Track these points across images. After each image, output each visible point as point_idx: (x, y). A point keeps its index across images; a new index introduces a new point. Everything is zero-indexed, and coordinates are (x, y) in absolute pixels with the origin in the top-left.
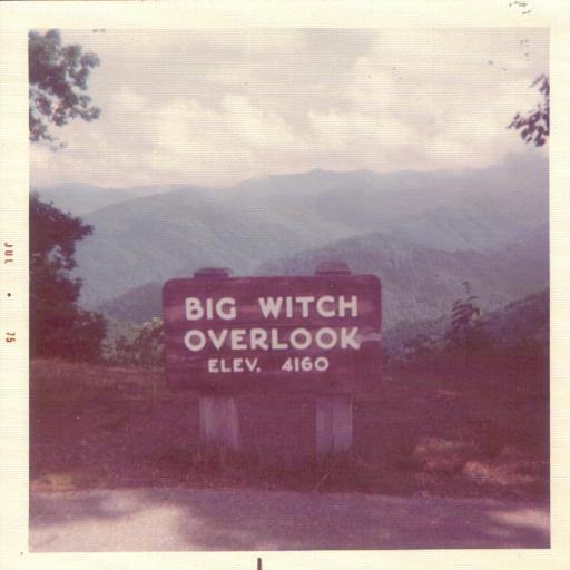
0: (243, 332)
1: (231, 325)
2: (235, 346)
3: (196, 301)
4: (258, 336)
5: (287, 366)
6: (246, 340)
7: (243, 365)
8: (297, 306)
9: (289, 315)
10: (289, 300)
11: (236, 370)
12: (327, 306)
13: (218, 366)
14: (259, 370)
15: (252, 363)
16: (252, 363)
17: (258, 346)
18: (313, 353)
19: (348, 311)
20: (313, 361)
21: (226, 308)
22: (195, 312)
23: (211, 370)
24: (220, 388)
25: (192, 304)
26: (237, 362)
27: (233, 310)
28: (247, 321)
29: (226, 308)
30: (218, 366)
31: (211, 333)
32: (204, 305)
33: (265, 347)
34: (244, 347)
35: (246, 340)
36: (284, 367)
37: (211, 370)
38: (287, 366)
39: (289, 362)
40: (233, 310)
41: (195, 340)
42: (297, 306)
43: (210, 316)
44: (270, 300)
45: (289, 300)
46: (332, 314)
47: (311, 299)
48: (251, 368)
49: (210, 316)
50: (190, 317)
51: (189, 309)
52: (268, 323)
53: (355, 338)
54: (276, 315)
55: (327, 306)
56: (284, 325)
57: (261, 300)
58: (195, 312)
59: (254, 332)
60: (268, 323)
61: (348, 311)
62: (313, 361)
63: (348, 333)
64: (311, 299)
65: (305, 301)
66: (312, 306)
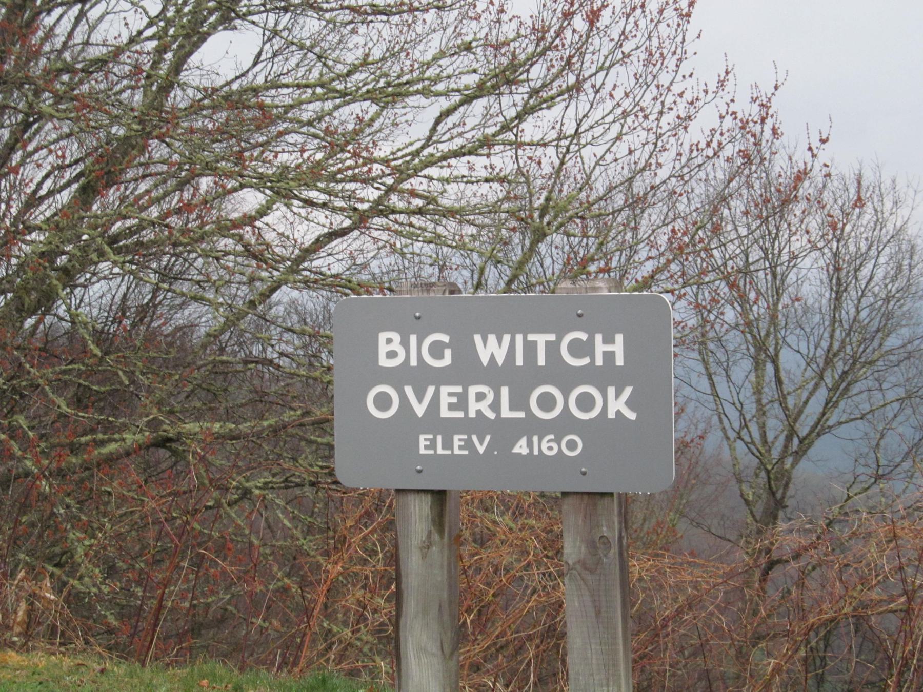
0: (459, 389)
1: (441, 377)
2: (445, 413)
3: (396, 337)
4: (480, 397)
5: (521, 448)
6: (461, 403)
7: (468, 445)
8: (531, 348)
9: (519, 362)
10: (519, 338)
11: (457, 451)
12: (577, 349)
13: (432, 445)
14: (99, 212)
15: (481, 442)
16: (481, 442)
17: (479, 412)
18: (566, 424)
19: (609, 357)
20: (558, 441)
21: (437, 350)
22: (392, 355)
23: (422, 451)
24: (222, 331)
25: (389, 341)
26: (458, 440)
27: (448, 353)
28: (467, 370)
29: (437, 350)
30: (432, 445)
31: (409, 390)
32: (405, 343)
33: (491, 415)
34: (460, 414)
35: (461, 403)
36: (516, 450)
37: (422, 451)
38: (521, 448)
39: (523, 441)
40: (448, 353)
41: (383, 402)
42: (531, 348)
43: (414, 362)
44: (492, 338)
45: (519, 338)
46: (586, 361)
47: (552, 337)
48: (481, 449)
49: (414, 362)
50: (384, 362)
51: (383, 349)
52: (494, 375)
53: (629, 404)
54: (500, 361)
55: (577, 349)
56: (517, 378)
57: (478, 338)
58: (392, 355)
59: (473, 390)
60: (494, 375)
61: (609, 357)
62: (558, 441)
63: (617, 396)
64: (552, 337)
65: (541, 339)
66: (552, 349)
